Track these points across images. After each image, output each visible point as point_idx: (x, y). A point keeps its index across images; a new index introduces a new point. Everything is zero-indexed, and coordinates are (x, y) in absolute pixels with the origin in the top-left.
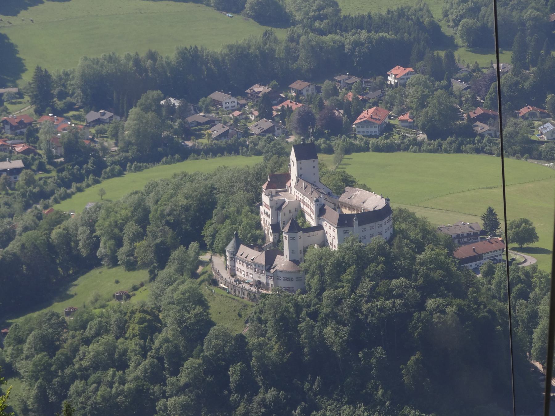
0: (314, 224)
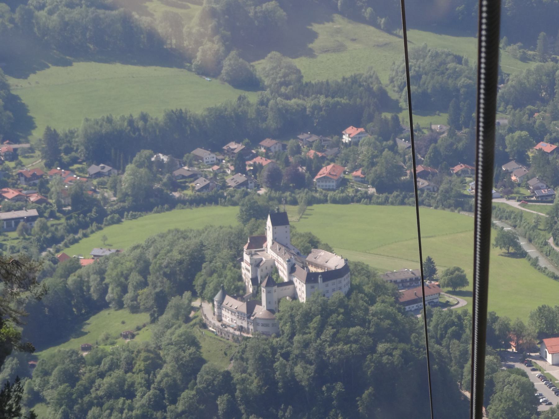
0: (286, 280)
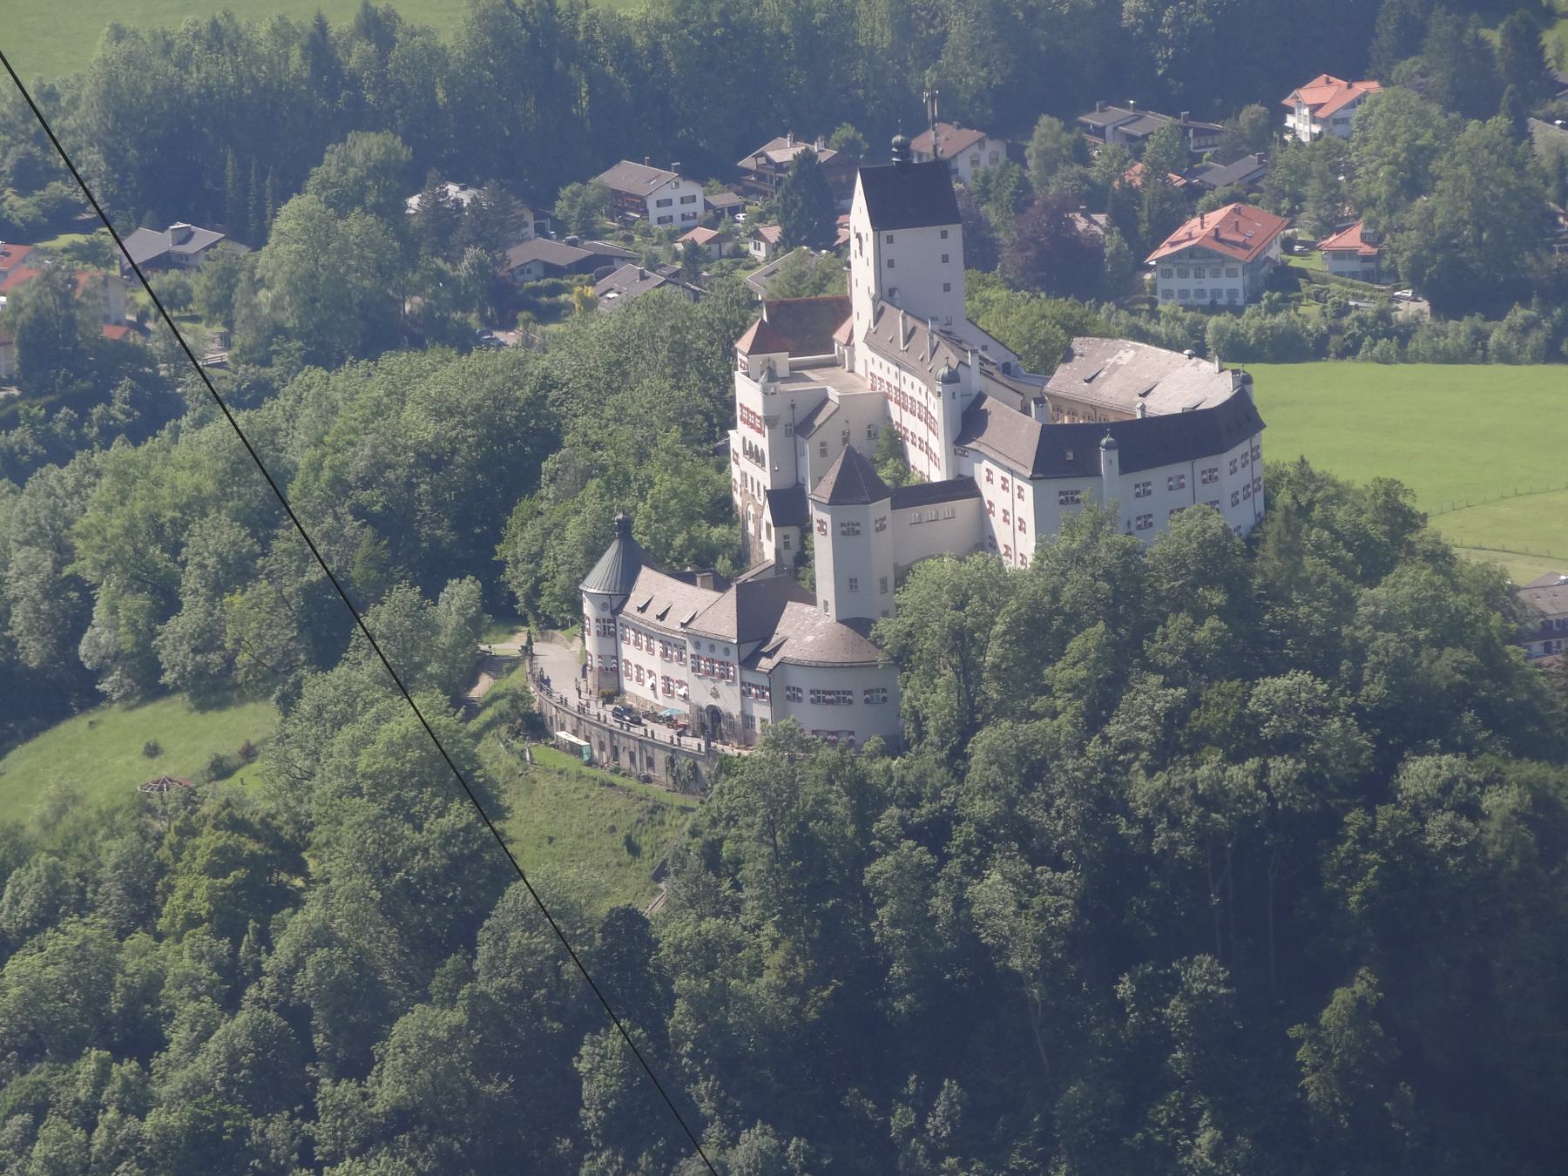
0: (937, 475)
